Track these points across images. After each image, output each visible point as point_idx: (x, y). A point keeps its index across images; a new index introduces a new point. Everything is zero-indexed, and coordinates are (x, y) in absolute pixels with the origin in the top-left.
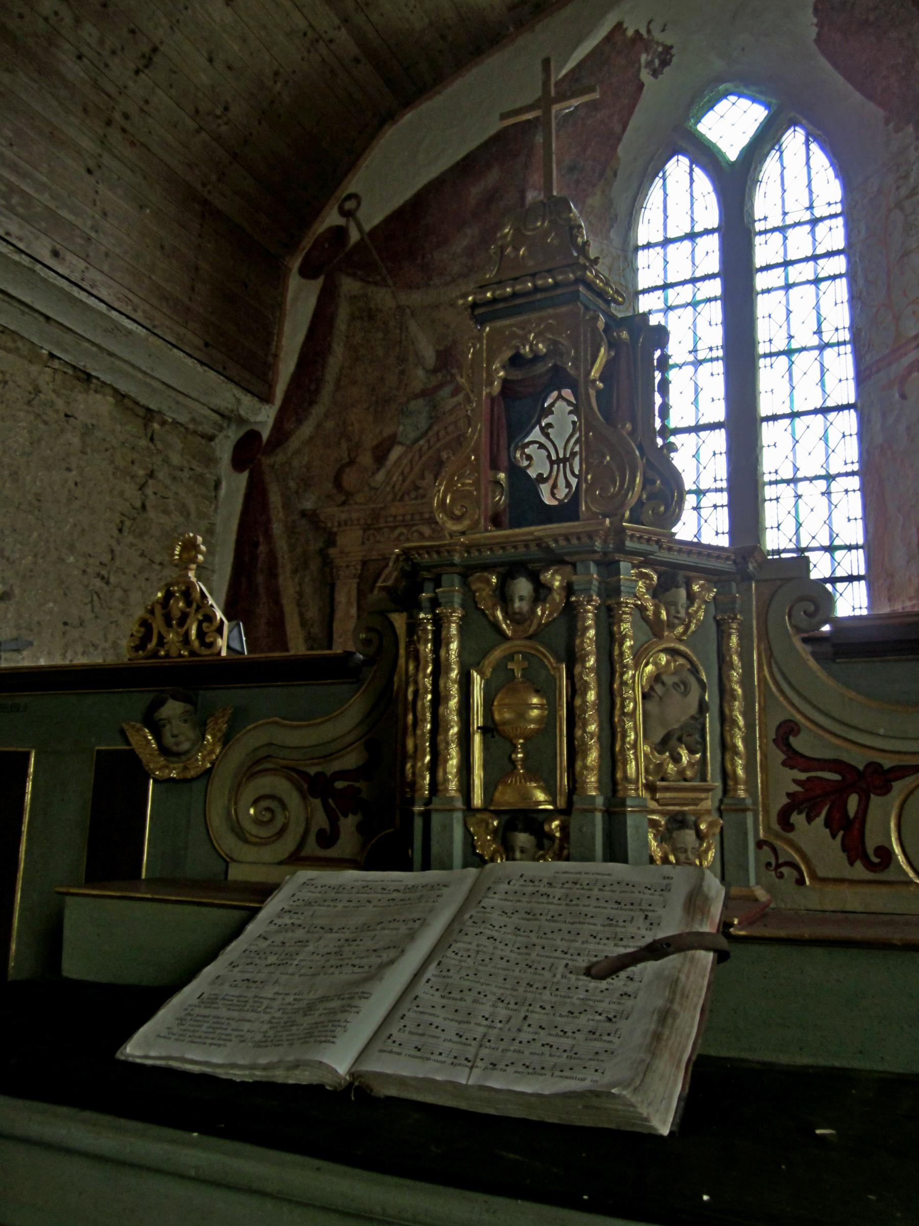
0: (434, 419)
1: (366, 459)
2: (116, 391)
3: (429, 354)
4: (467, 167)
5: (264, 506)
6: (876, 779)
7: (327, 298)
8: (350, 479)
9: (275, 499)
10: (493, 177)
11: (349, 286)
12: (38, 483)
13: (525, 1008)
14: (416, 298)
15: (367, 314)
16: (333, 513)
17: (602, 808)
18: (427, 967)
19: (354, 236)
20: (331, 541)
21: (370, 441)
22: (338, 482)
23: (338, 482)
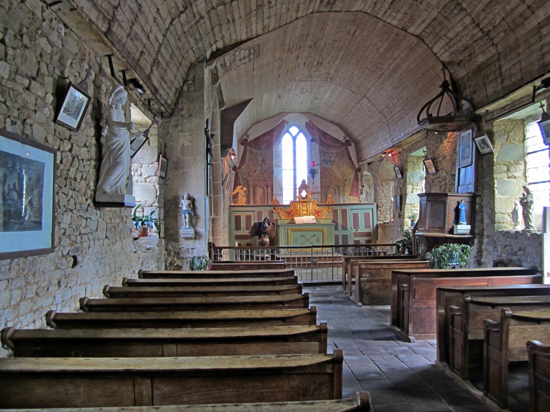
0: (262, 168)
1: (253, 172)
2: (104, 15)
3: (261, 159)
4: (265, 135)
5: (238, 176)
6: (319, 212)
7: (245, 148)
8: (251, 174)
9: (240, 175)
10: (268, 137)
11: (248, 148)
12: (267, 240)
13: (80, 227)
14: (258, 151)
15: (251, 152)
16: (248, 178)
17: (144, 383)
18: (257, 285)
19: (249, 141)
20: (249, 182)
21: (253, 170)
22: (249, 174)
23: (249, 174)
